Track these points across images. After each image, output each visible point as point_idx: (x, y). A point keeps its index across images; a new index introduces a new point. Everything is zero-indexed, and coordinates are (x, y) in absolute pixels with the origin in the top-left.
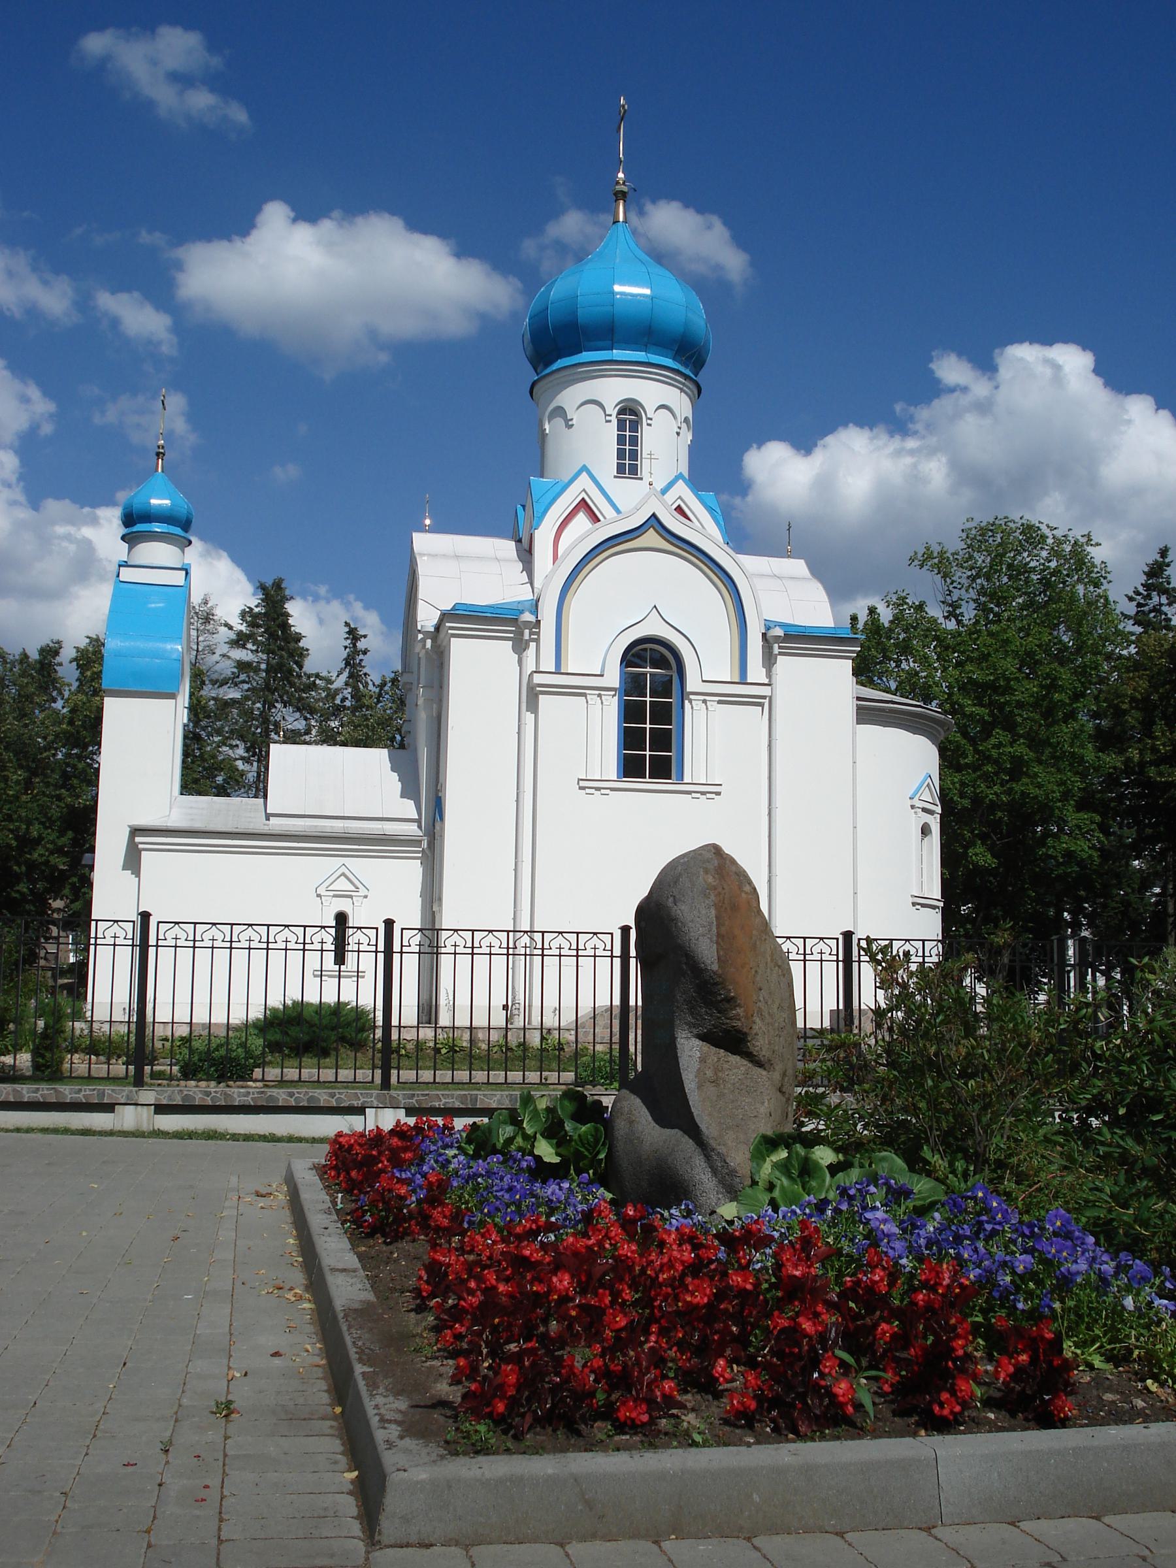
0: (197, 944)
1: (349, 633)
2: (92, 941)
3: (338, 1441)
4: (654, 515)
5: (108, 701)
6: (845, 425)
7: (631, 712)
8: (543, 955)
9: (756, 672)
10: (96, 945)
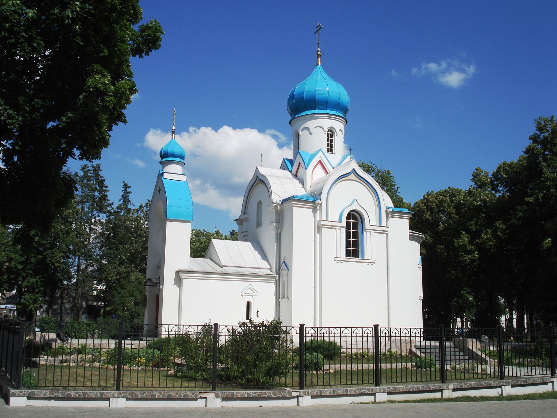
1: (124, 185)
2: (422, 335)
4: (354, 169)
5: (168, 223)
7: (348, 235)
9: (384, 224)
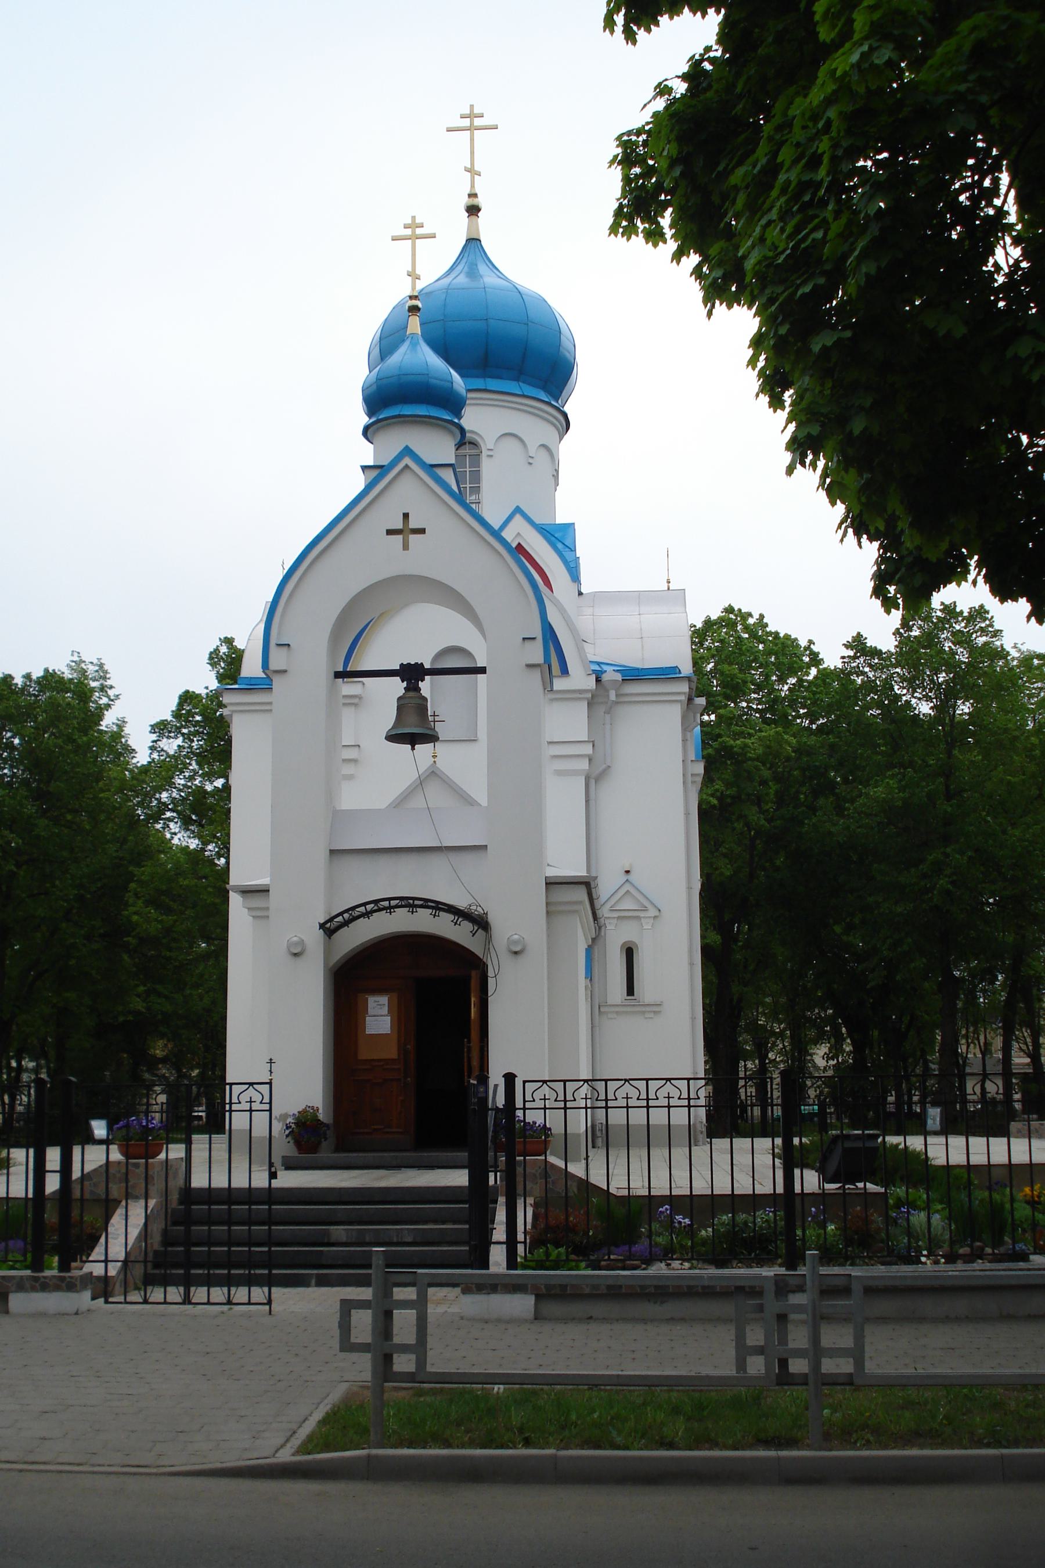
0: (569, 1104)
2: (227, 1107)
3: (155, 1289)
6: (674, 10)
8: (607, 1108)
10: (231, 1111)
